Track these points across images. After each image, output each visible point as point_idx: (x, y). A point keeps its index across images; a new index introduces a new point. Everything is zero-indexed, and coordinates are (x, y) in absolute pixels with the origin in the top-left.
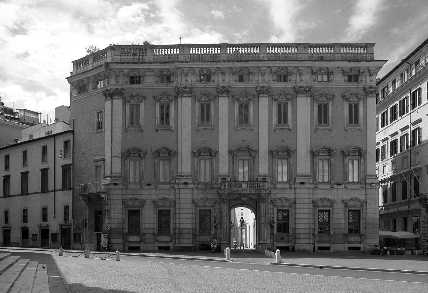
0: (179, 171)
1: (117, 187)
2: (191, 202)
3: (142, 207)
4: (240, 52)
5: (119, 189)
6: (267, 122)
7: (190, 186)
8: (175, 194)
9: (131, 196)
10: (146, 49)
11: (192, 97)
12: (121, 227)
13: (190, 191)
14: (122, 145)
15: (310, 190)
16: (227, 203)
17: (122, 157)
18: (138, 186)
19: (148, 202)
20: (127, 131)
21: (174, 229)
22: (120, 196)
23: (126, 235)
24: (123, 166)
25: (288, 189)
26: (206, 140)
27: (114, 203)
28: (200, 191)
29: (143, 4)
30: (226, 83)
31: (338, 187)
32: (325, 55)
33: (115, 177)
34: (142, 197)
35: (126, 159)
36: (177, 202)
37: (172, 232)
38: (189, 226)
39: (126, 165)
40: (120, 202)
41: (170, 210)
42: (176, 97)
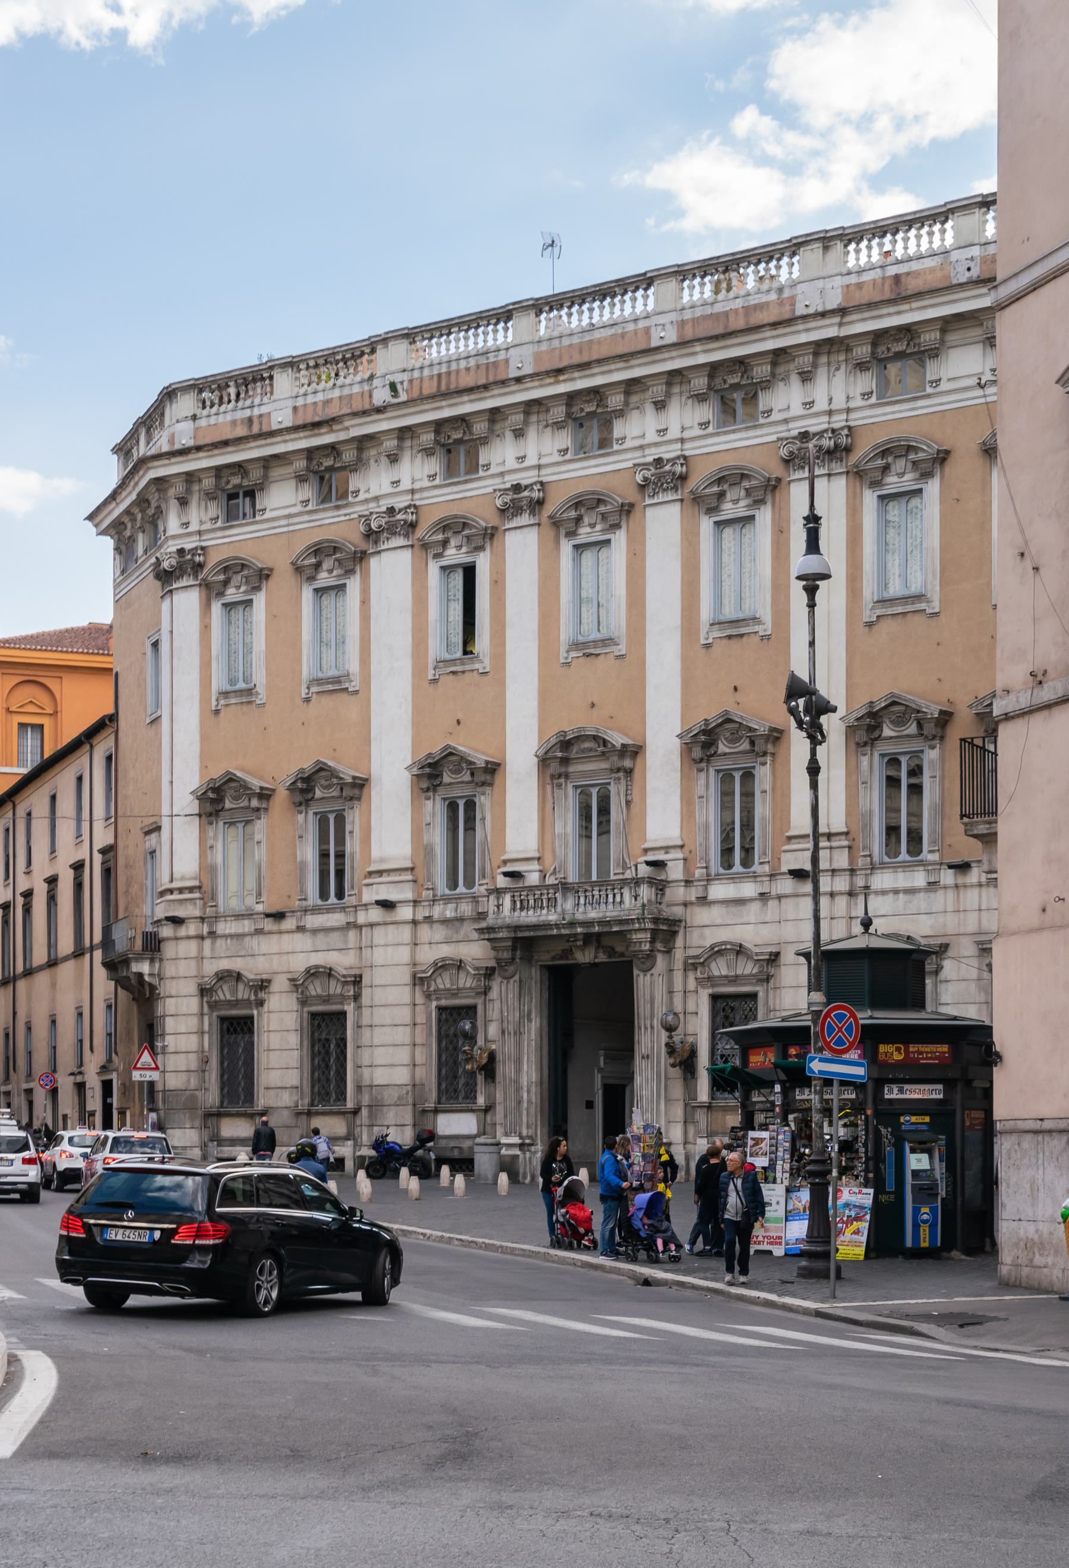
0: (375, 853)
1: (182, 931)
2: (407, 978)
3: (260, 1003)
4: (899, 253)
5: (189, 938)
6: (404, 641)
7: (405, 913)
8: (361, 948)
9: (225, 965)
10: (271, 378)
11: (416, 548)
12: (193, 1083)
13: (406, 933)
14: (201, 770)
15: (838, 899)
16: (517, 977)
17: (200, 815)
18: (247, 926)
19: (280, 984)
20: (217, 712)
21: (359, 1088)
22: (193, 963)
23: (213, 1116)
24: (205, 848)
25: (752, 900)
26: (460, 716)
27: (174, 993)
28: (439, 933)
29: (825, 23)
30: (817, 414)
31: (960, 881)
32: (914, 266)
33: (181, 890)
34: (251, 968)
35: (617, 775)
36: (365, 981)
37: (350, 1104)
38: (401, 1076)
39: (210, 842)
40: (192, 988)
41: (343, 1014)
42: (361, 557)
